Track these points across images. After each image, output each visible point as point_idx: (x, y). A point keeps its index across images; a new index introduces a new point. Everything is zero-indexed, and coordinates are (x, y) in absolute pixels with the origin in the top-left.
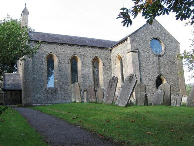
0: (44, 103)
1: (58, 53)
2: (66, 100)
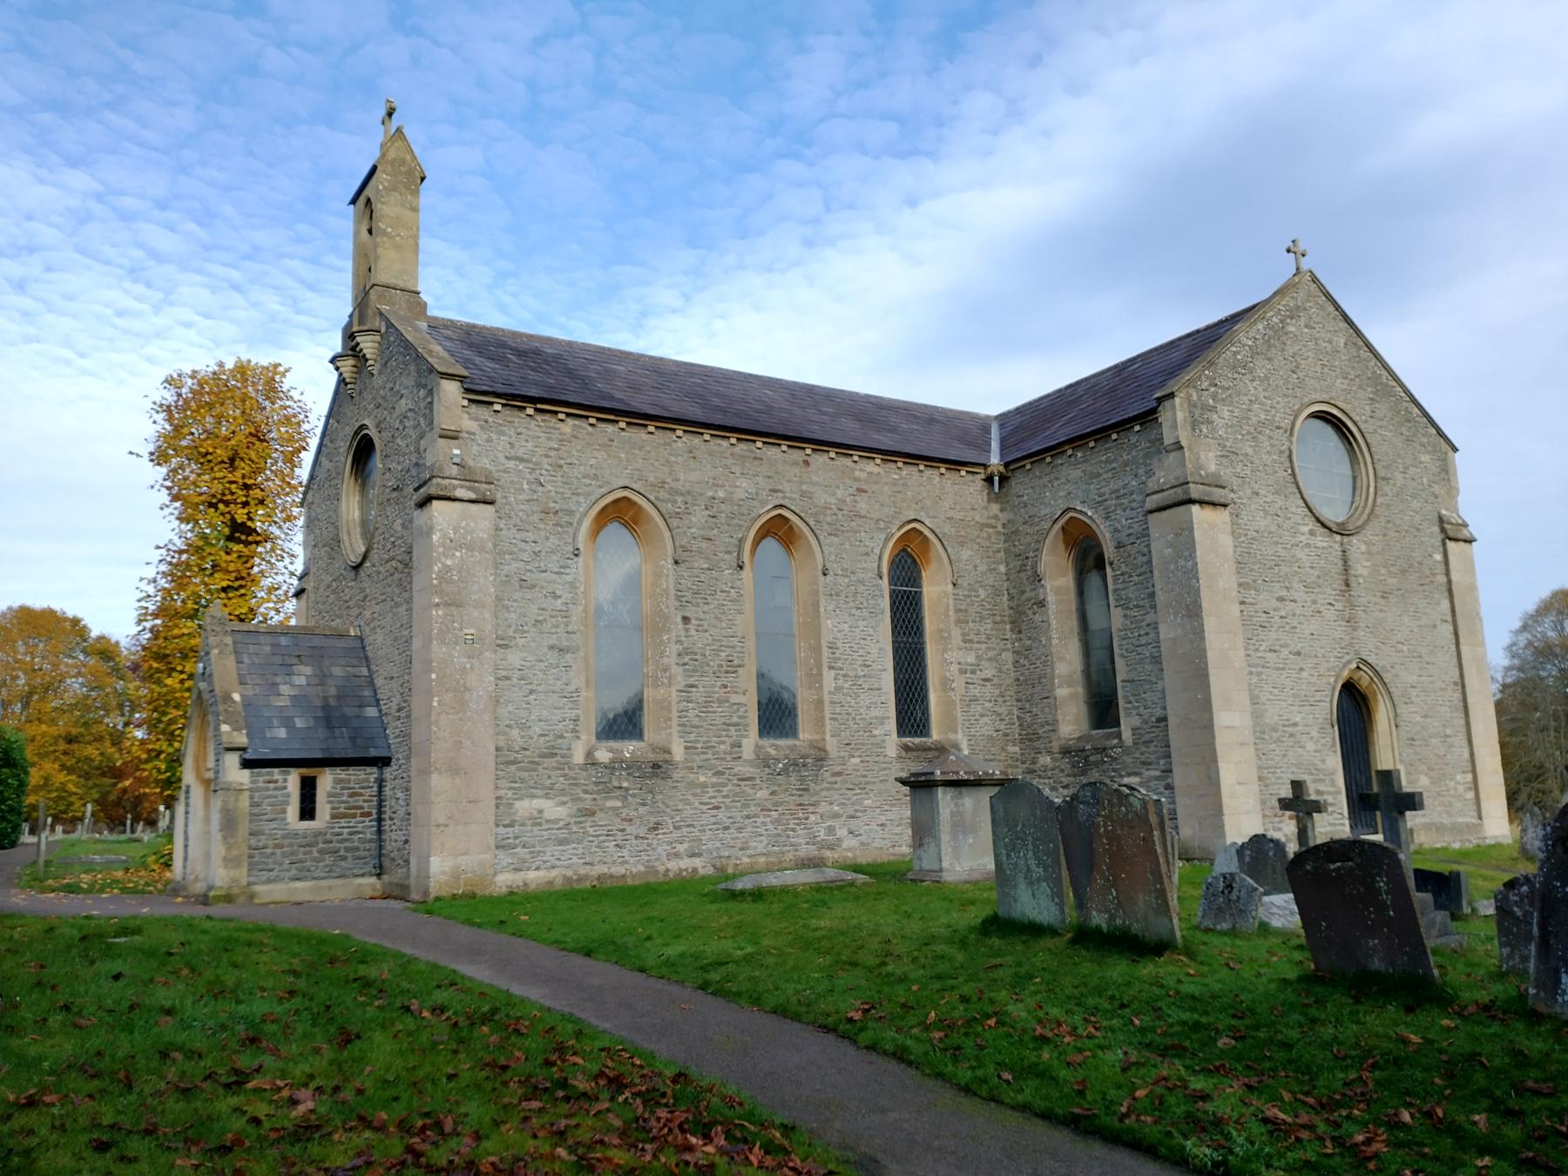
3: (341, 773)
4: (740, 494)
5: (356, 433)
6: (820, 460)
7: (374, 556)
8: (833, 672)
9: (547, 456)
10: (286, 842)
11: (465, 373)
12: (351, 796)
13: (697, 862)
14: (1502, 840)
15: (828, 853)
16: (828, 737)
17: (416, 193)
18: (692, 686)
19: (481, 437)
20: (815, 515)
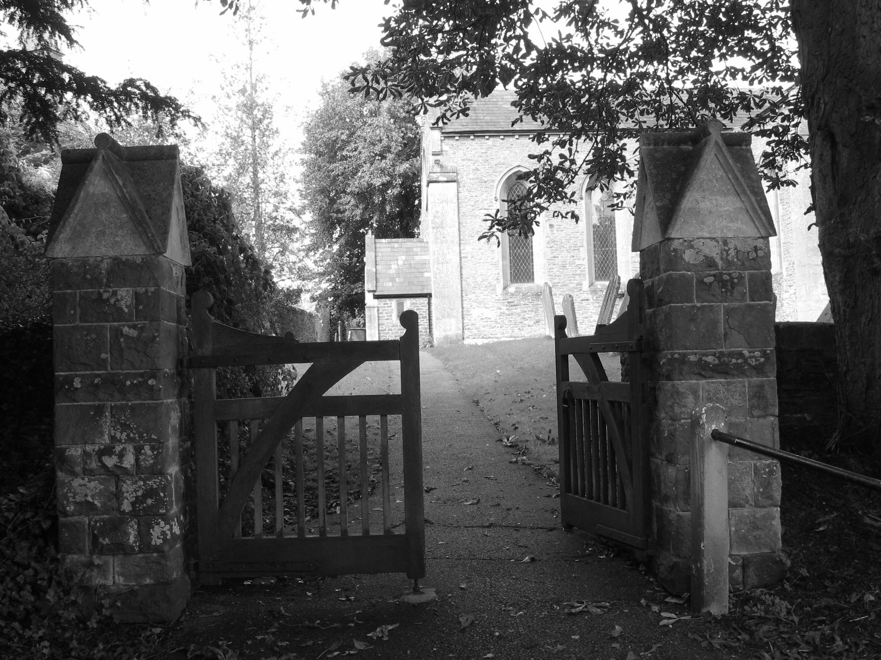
0: (499, 335)
14: (42, 189)
19: (451, 152)
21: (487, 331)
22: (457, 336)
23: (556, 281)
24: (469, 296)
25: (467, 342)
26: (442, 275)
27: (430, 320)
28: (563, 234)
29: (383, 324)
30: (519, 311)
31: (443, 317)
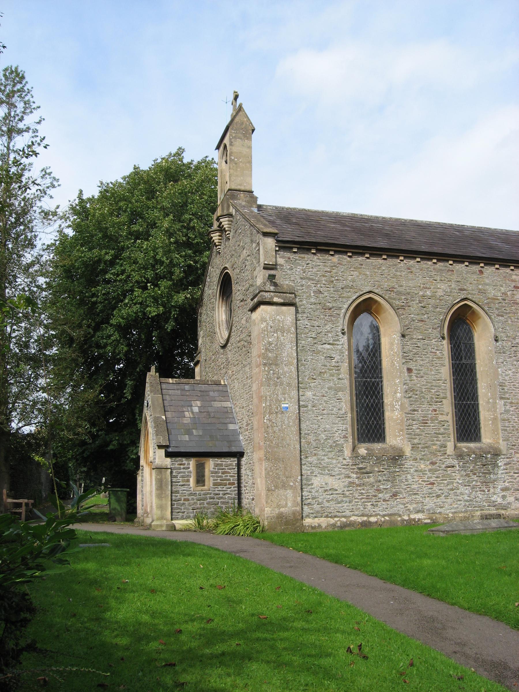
0: (348, 513)
1: (399, 293)
2: (438, 496)
3: (219, 461)
4: (440, 293)
5: (222, 273)
6: (489, 270)
7: (232, 340)
8: (503, 402)
9: (324, 276)
10: (190, 498)
11: (276, 231)
12: (223, 473)
13: (420, 516)
15: (503, 512)
16: (501, 441)
17: (249, 139)
18: (414, 410)
20: (488, 304)
21: (333, 507)
22: (294, 513)
23: (416, 441)
24: (309, 459)
25: (307, 521)
26: (275, 429)
27: (239, 487)
28: (423, 381)
29: (177, 492)
30: (372, 480)
31: (276, 487)
